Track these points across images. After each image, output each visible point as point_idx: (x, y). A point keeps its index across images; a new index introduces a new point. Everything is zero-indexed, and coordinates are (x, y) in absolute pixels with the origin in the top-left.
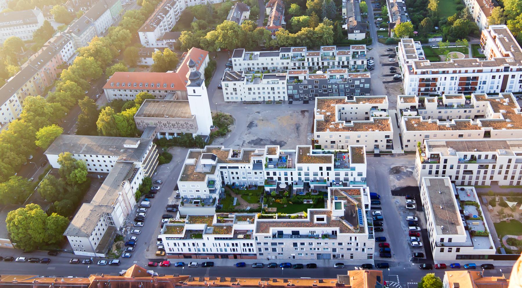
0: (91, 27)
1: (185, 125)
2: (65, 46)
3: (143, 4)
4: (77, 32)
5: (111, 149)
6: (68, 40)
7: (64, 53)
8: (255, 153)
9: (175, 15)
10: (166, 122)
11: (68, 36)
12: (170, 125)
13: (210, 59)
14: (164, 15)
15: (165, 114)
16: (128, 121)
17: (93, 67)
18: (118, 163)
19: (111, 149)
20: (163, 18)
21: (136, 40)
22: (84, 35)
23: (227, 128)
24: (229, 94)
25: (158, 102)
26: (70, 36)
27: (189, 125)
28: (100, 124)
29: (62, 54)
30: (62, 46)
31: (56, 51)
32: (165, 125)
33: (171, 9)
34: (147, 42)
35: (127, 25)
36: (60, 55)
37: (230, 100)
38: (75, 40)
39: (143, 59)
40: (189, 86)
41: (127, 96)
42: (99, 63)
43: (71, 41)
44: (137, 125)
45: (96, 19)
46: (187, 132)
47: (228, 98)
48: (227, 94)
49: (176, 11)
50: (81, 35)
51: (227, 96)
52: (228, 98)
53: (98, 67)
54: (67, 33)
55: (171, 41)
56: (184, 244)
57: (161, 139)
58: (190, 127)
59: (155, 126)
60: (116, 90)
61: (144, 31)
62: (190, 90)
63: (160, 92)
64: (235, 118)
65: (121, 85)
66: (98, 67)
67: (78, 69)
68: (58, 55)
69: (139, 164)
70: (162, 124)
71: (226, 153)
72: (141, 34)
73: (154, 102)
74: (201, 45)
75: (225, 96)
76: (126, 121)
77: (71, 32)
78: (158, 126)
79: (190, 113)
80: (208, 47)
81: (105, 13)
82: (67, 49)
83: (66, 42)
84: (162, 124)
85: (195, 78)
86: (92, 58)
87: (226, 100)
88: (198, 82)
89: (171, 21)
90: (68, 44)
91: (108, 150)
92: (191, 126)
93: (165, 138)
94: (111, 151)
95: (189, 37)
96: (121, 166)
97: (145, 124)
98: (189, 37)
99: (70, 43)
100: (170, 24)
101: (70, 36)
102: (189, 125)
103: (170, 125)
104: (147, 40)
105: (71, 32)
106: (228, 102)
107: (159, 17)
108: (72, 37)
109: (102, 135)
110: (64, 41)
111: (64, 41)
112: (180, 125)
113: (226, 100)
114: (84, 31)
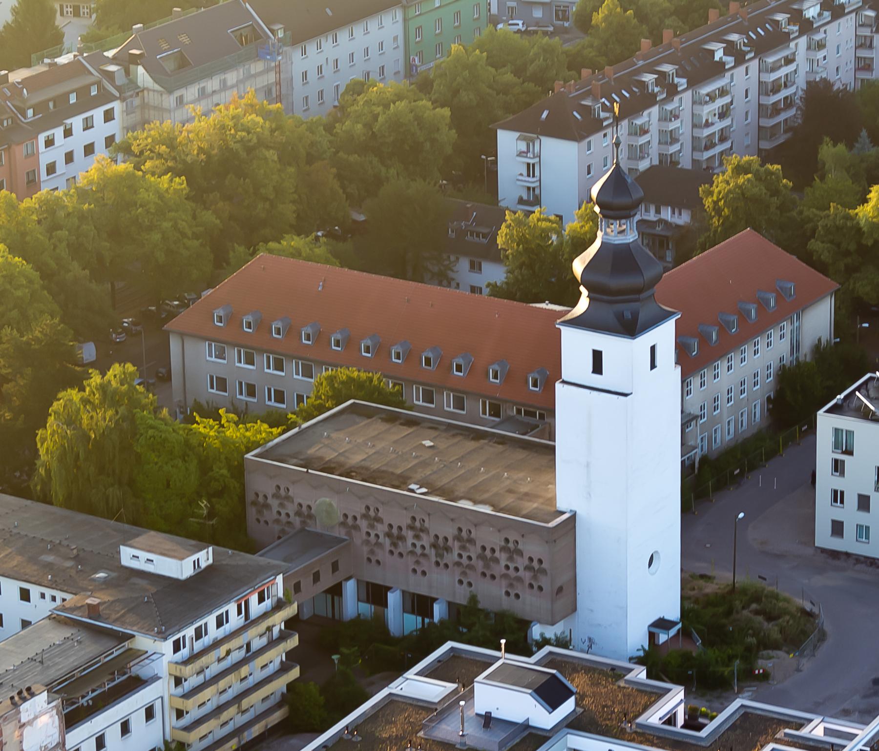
0: (257, 67)
1: (503, 557)
2: (77, 122)
3: (598, 18)
4: (170, 66)
5: (50, 558)
6: (104, 97)
7: (56, 155)
8: (804, 732)
9: (762, 110)
10: (405, 521)
11: (110, 76)
12: (426, 540)
13: (839, 327)
14: (682, 82)
15: (418, 476)
16: (205, 466)
17: (166, 225)
18: (55, 619)
19: (50, 558)
20: (672, 91)
21: (477, 170)
22: (203, 94)
23: (750, 655)
24: (851, 500)
25: (411, 422)
26: (120, 80)
27: (521, 563)
28: (49, 440)
29: (46, 157)
30: (56, 113)
31: (16, 126)
32: (397, 539)
33: (740, 60)
34: (533, 199)
35: (456, 92)
36: (34, 155)
37: (848, 544)
38: (144, 106)
39: (464, 264)
40: (578, 323)
41: (280, 397)
42: (208, 216)
43: (117, 106)
44: (252, 513)
45: (301, 36)
46: (507, 604)
47: (837, 528)
48: (838, 497)
49: (776, 88)
50: (186, 84)
51: (838, 513)
52: (837, 528)
53: (196, 236)
54: (114, 60)
55: (667, 214)
56: (43, 596)
57: (358, 621)
58: (527, 576)
59: (340, 533)
60: (233, 353)
61: (533, 128)
62: (577, 347)
63: (459, 405)
64: (828, 627)
65: (262, 326)
66: (196, 236)
67: (83, 217)
68: (20, 151)
69: (160, 654)
70: (381, 529)
71: (644, 700)
72: (508, 142)
73: (392, 418)
74: (815, 245)
75: (825, 512)
76: (193, 466)
77: (135, 60)
78: (358, 538)
79: (552, 500)
80: (851, 270)
81: (373, 24)
82: (80, 138)
83: (86, 103)
84: (381, 529)
85: (616, 283)
86: (180, 183)
87: (823, 538)
88: (627, 310)
89: (719, 125)
90: (98, 114)
91: (33, 560)
92: (536, 568)
93: (380, 621)
94: (49, 566)
95: (759, 190)
96: (57, 636)
97: (291, 509)
98: (759, 190)
99: (109, 116)
100: (710, 146)
101: (120, 80)
102: (521, 563)
103: (426, 540)
104: (532, 182)
105: (135, 60)
106: (835, 554)
107: (649, 78)
108: (129, 90)
109: (46, 499)
110: (83, 92)
111: (83, 92)
112: (474, 551)
113: (823, 538)
114: (209, 74)
